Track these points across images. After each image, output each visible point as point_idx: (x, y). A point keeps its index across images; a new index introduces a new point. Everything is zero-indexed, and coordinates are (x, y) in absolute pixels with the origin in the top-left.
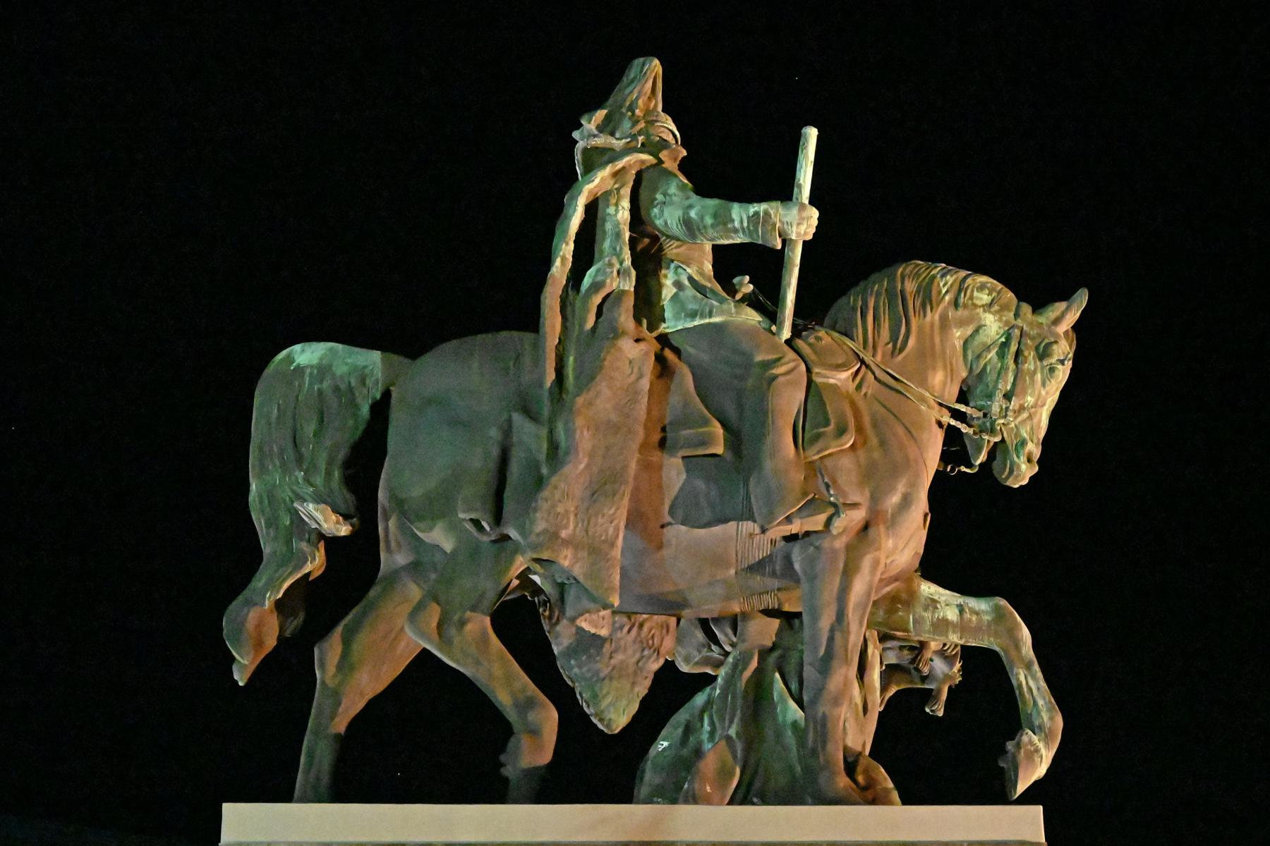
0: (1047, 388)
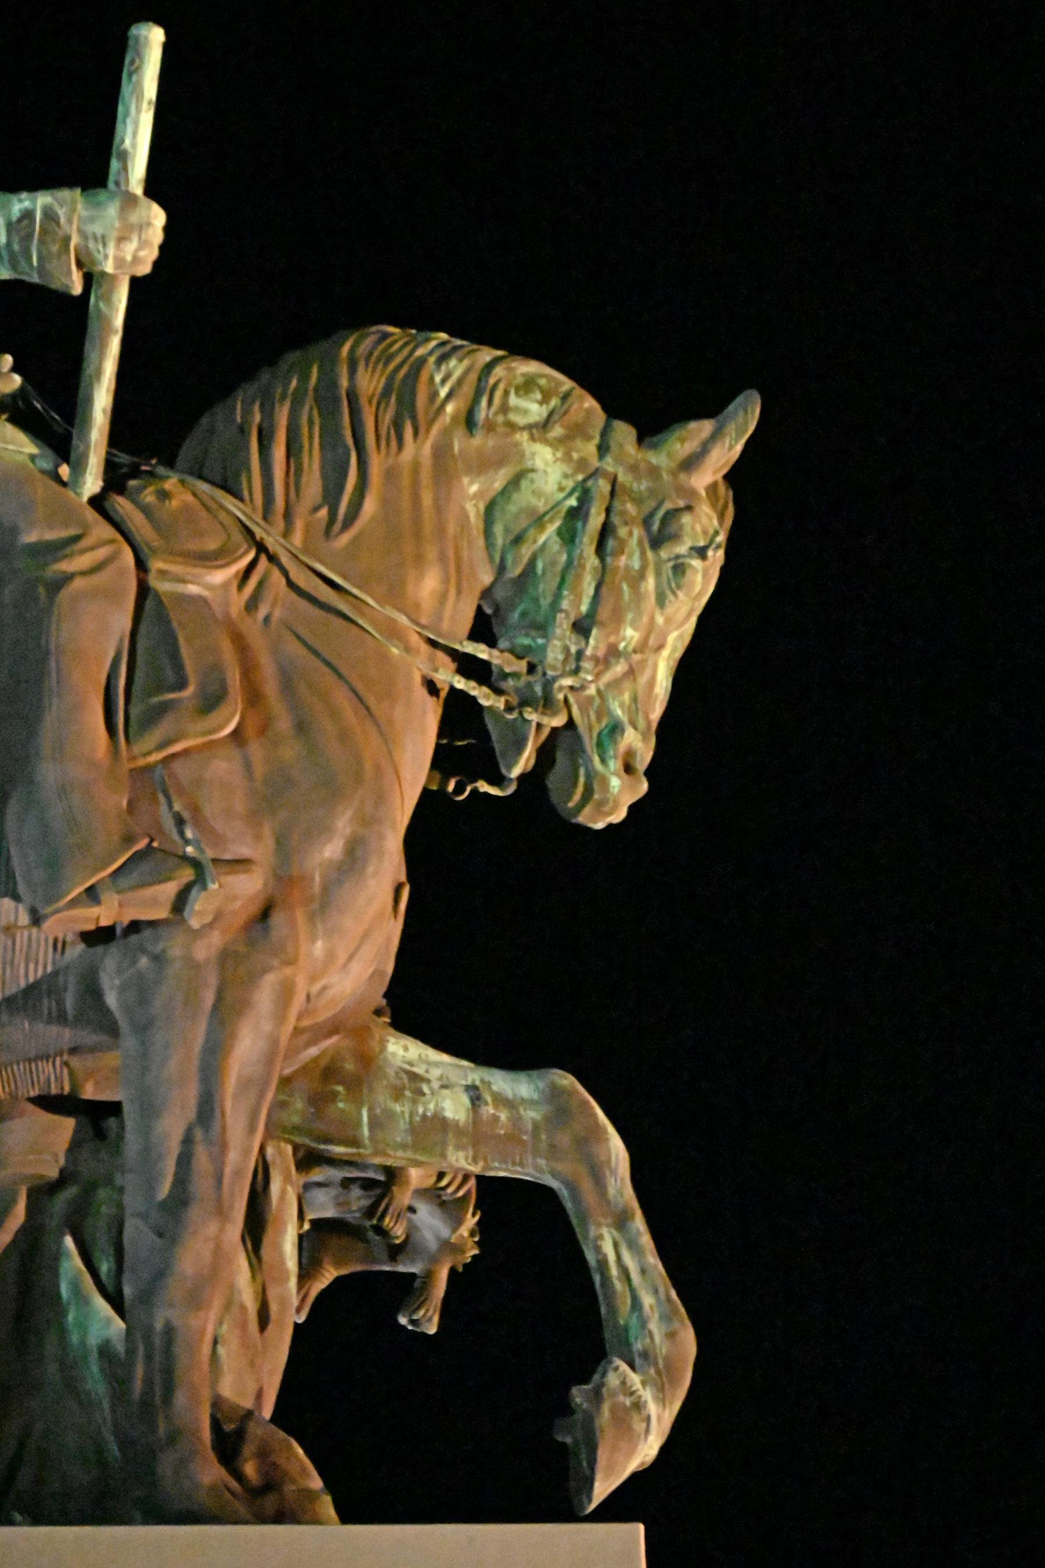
0: (669, 610)
